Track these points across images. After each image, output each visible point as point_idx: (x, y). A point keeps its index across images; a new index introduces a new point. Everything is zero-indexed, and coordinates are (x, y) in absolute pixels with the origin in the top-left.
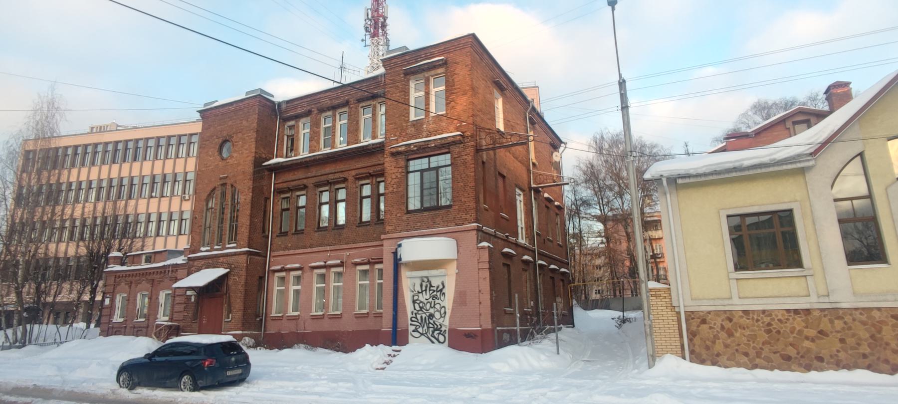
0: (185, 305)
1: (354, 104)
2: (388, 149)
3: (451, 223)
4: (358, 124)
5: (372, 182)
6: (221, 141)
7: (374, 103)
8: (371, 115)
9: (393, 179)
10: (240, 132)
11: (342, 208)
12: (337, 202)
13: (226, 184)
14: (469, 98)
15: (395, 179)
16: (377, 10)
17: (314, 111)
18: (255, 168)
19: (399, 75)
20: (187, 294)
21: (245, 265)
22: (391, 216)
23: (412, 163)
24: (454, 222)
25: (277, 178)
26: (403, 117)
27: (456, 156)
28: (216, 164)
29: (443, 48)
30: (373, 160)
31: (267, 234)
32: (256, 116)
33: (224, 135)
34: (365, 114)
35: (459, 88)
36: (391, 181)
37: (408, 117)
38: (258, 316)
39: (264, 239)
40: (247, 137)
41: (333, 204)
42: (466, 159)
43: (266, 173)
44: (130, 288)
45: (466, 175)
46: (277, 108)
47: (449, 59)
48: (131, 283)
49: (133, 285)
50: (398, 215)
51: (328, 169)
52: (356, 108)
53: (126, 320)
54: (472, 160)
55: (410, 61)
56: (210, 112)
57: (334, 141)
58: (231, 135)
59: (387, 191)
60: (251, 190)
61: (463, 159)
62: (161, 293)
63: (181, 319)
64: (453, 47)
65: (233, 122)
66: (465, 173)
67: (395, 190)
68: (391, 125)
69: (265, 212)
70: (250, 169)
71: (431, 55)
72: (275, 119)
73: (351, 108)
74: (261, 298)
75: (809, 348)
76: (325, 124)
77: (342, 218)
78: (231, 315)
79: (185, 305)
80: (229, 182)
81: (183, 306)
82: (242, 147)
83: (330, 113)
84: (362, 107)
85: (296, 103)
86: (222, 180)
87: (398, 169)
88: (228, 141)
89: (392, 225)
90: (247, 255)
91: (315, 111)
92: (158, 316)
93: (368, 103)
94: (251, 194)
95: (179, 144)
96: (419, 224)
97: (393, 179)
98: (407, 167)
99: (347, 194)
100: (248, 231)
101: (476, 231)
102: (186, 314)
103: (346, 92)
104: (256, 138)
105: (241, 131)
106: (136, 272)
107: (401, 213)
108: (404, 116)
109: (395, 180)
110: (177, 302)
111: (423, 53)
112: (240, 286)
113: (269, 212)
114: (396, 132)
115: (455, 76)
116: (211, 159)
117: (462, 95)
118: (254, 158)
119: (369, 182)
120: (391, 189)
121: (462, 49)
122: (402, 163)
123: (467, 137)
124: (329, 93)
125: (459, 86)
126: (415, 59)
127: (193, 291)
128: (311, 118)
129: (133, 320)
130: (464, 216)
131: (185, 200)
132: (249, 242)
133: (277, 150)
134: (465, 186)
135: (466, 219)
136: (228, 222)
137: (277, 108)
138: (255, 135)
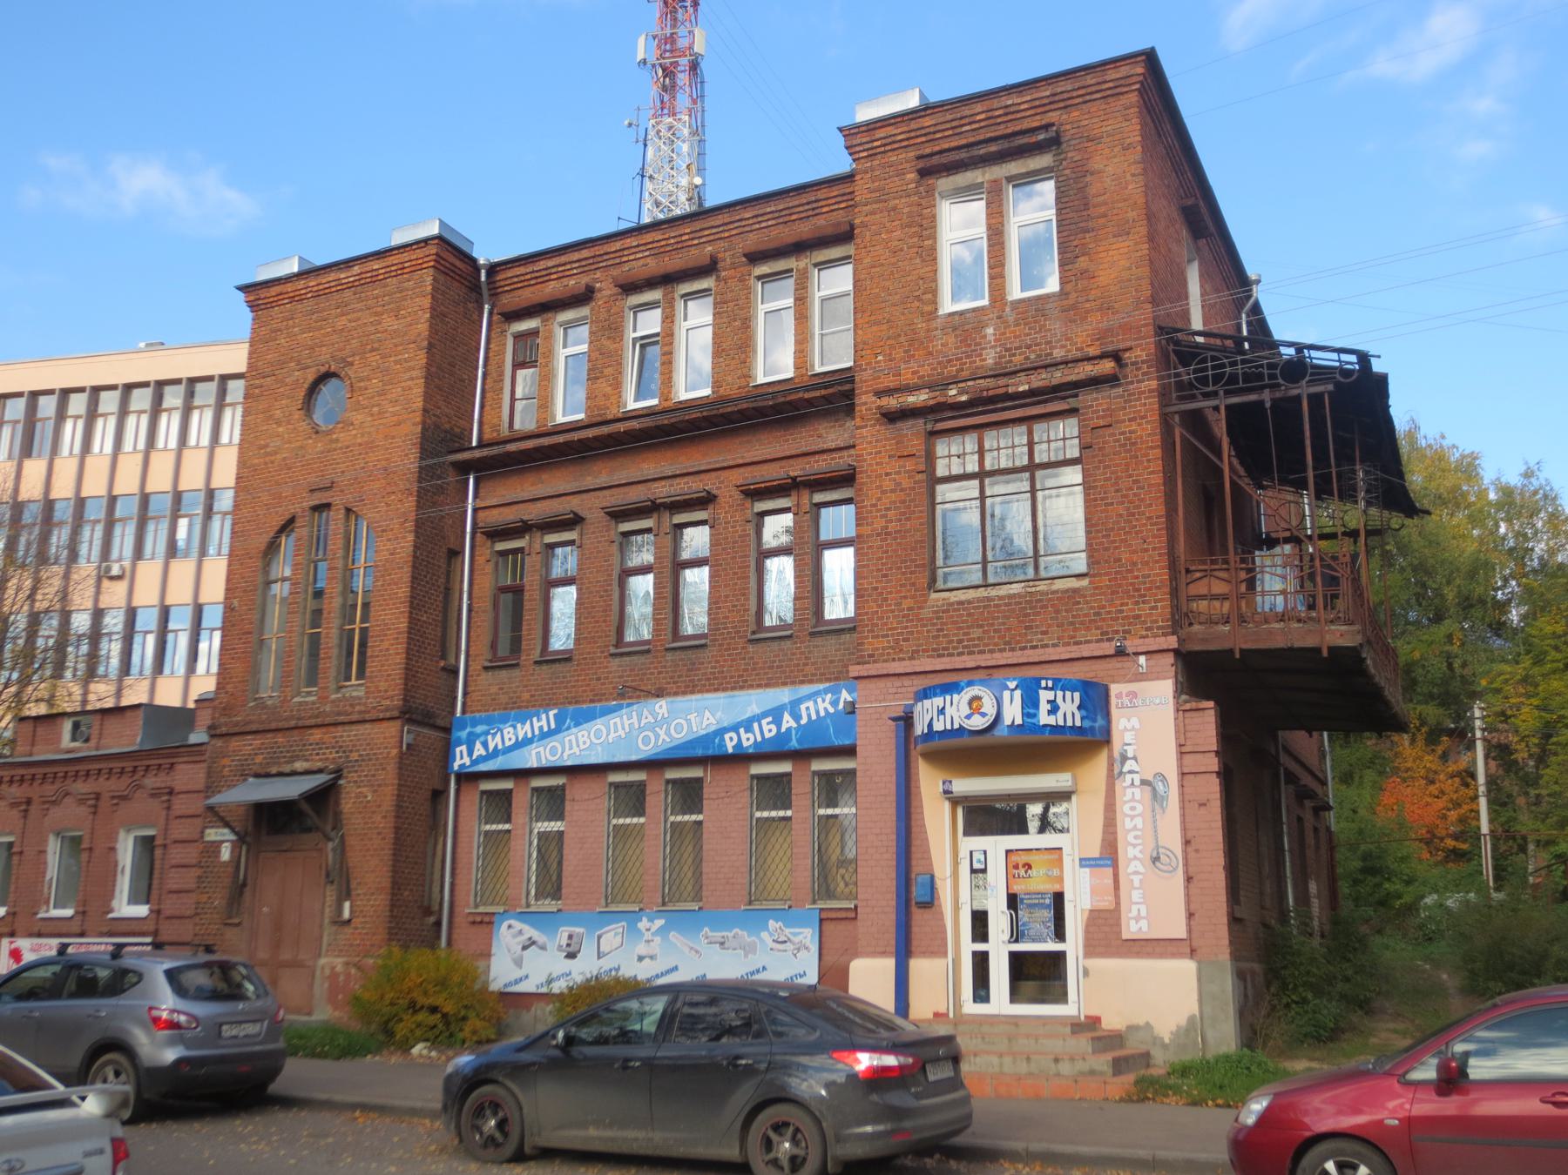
0: (199, 872)
1: (734, 266)
2: (866, 402)
3: (1088, 629)
4: (749, 327)
5: (798, 505)
6: (311, 376)
7: (802, 264)
8: (792, 300)
9: (884, 492)
10: (373, 350)
11: (697, 580)
12: (681, 565)
13: (328, 506)
14: (1136, 244)
15: (892, 491)
16: (671, 39)
17: (600, 290)
18: (421, 459)
19: (900, 174)
20: (207, 838)
21: (395, 752)
22: (880, 606)
23: (941, 448)
24: (1097, 628)
25: (482, 492)
26: (917, 304)
27: (1102, 423)
28: (298, 444)
29: (1048, 93)
30: (830, 434)
31: (452, 661)
32: (427, 302)
33: (322, 358)
34: (822, 287)
35: (1105, 216)
36: (879, 499)
37: (934, 302)
38: (428, 911)
39: (444, 675)
40: (396, 362)
41: (667, 572)
42: (1131, 432)
43: (452, 478)
44: (25, 817)
45: (1135, 482)
46: (483, 278)
47: (1068, 127)
48: (29, 802)
49: (33, 808)
50: (906, 604)
51: (649, 465)
52: (742, 280)
53: (14, 914)
54: (1155, 434)
55: (935, 133)
56: (278, 289)
57: (670, 379)
58: (343, 360)
59: (867, 530)
60: (410, 525)
61: (1123, 433)
62: (122, 834)
63: (188, 913)
64: (1080, 92)
65: (350, 321)
66: (1130, 476)
67: (892, 527)
68: (875, 328)
69: (448, 591)
70: (407, 460)
71: (1006, 114)
72: (475, 317)
73: (725, 281)
74: (434, 854)
75: (649, 1059)
76: (635, 331)
77: (695, 618)
78: (347, 905)
79: (199, 872)
80: (337, 500)
81: (195, 872)
82: (382, 393)
83: (655, 295)
84: (759, 278)
85: (542, 264)
86: (318, 495)
87: (901, 462)
88: (334, 375)
89: (887, 636)
90: (398, 723)
91: (606, 289)
92: (115, 904)
93: (781, 265)
94: (411, 537)
95: (92, 415)
96: (976, 633)
97: (884, 492)
98: (931, 458)
99: (715, 542)
100: (402, 648)
101: (1172, 654)
102: (204, 898)
103: (706, 233)
104: (429, 365)
105: (376, 345)
106: (33, 771)
107: (913, 597)
108: (918, 298)
109: (893, 497)
110: (174, 862)
111: (978, 108)
112: (378, 818)
113: (457, 595)
114: (892, 347)
115: (1088, 178)
116: (281, 429)
117: (1114, 236)
118: (419, 428)
119: (789, 505)
120: (879, 524)
121: (1113, 95)
122: (916, 444)
123: (1133, 364)
124: (653, 234)
125: (1103, 209)
126: (952, 128)
127: (226, 831)
128: (592, 310)
129: (36, 914)
130: (1129, 608)
131: (112, 578)
132: (406, 684)
133: (482, 407)
134: (1133, 515)
135: (1138, 616)
136: (336, 623)
137: (483, 278)
138: (421, 357)
